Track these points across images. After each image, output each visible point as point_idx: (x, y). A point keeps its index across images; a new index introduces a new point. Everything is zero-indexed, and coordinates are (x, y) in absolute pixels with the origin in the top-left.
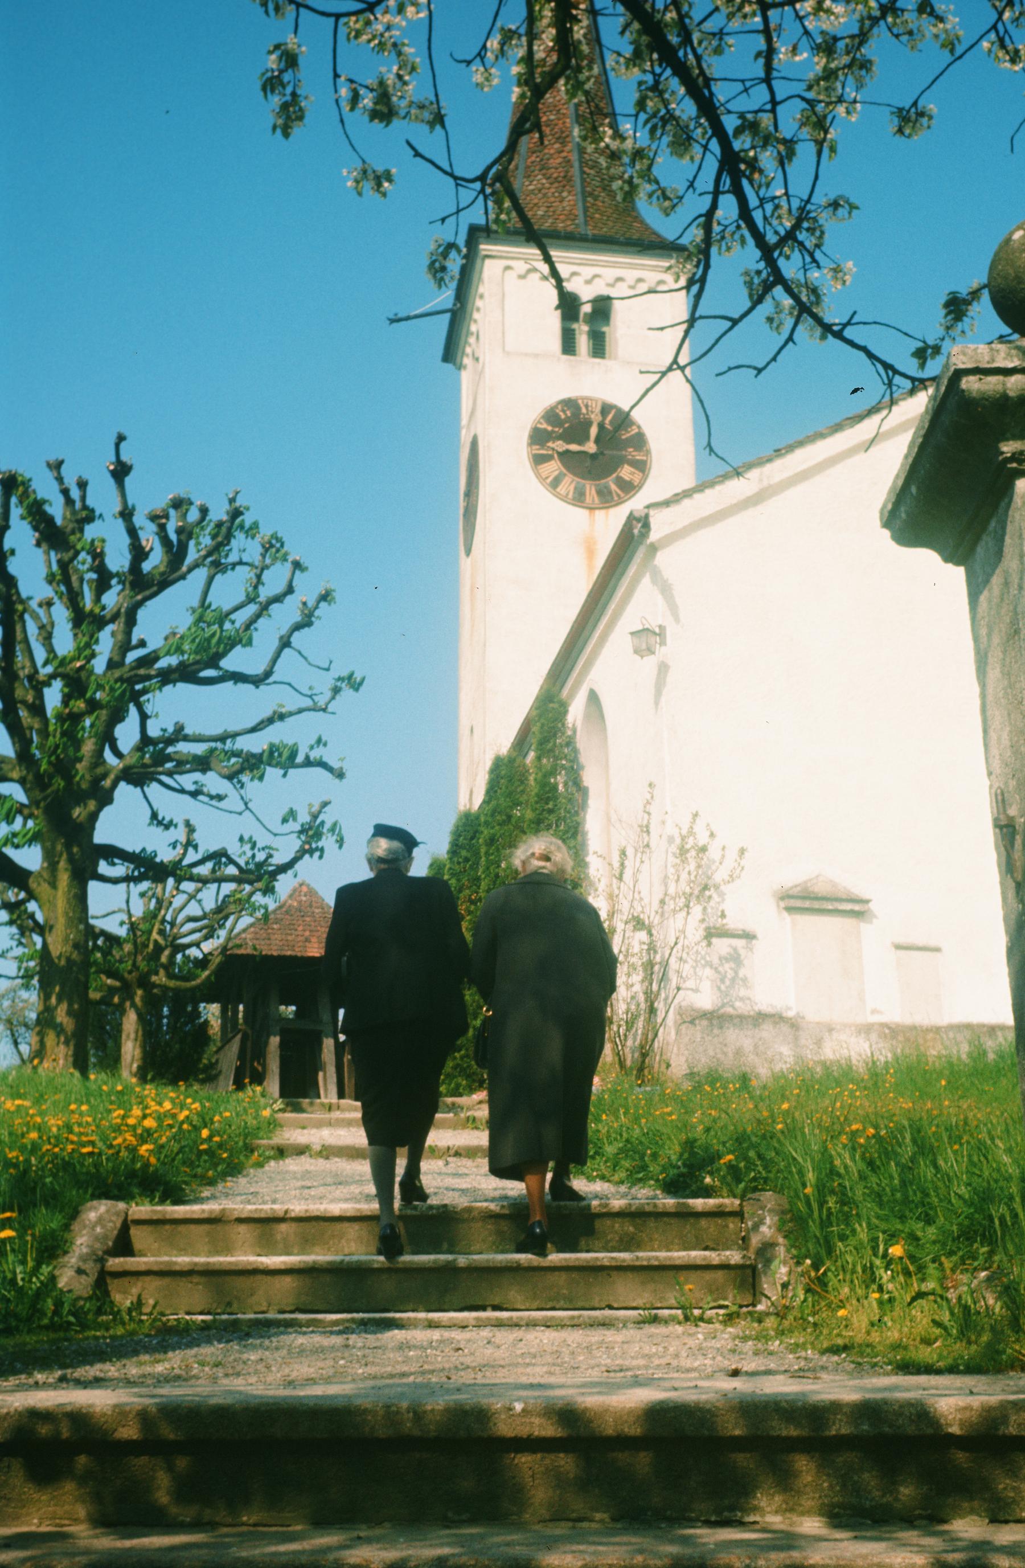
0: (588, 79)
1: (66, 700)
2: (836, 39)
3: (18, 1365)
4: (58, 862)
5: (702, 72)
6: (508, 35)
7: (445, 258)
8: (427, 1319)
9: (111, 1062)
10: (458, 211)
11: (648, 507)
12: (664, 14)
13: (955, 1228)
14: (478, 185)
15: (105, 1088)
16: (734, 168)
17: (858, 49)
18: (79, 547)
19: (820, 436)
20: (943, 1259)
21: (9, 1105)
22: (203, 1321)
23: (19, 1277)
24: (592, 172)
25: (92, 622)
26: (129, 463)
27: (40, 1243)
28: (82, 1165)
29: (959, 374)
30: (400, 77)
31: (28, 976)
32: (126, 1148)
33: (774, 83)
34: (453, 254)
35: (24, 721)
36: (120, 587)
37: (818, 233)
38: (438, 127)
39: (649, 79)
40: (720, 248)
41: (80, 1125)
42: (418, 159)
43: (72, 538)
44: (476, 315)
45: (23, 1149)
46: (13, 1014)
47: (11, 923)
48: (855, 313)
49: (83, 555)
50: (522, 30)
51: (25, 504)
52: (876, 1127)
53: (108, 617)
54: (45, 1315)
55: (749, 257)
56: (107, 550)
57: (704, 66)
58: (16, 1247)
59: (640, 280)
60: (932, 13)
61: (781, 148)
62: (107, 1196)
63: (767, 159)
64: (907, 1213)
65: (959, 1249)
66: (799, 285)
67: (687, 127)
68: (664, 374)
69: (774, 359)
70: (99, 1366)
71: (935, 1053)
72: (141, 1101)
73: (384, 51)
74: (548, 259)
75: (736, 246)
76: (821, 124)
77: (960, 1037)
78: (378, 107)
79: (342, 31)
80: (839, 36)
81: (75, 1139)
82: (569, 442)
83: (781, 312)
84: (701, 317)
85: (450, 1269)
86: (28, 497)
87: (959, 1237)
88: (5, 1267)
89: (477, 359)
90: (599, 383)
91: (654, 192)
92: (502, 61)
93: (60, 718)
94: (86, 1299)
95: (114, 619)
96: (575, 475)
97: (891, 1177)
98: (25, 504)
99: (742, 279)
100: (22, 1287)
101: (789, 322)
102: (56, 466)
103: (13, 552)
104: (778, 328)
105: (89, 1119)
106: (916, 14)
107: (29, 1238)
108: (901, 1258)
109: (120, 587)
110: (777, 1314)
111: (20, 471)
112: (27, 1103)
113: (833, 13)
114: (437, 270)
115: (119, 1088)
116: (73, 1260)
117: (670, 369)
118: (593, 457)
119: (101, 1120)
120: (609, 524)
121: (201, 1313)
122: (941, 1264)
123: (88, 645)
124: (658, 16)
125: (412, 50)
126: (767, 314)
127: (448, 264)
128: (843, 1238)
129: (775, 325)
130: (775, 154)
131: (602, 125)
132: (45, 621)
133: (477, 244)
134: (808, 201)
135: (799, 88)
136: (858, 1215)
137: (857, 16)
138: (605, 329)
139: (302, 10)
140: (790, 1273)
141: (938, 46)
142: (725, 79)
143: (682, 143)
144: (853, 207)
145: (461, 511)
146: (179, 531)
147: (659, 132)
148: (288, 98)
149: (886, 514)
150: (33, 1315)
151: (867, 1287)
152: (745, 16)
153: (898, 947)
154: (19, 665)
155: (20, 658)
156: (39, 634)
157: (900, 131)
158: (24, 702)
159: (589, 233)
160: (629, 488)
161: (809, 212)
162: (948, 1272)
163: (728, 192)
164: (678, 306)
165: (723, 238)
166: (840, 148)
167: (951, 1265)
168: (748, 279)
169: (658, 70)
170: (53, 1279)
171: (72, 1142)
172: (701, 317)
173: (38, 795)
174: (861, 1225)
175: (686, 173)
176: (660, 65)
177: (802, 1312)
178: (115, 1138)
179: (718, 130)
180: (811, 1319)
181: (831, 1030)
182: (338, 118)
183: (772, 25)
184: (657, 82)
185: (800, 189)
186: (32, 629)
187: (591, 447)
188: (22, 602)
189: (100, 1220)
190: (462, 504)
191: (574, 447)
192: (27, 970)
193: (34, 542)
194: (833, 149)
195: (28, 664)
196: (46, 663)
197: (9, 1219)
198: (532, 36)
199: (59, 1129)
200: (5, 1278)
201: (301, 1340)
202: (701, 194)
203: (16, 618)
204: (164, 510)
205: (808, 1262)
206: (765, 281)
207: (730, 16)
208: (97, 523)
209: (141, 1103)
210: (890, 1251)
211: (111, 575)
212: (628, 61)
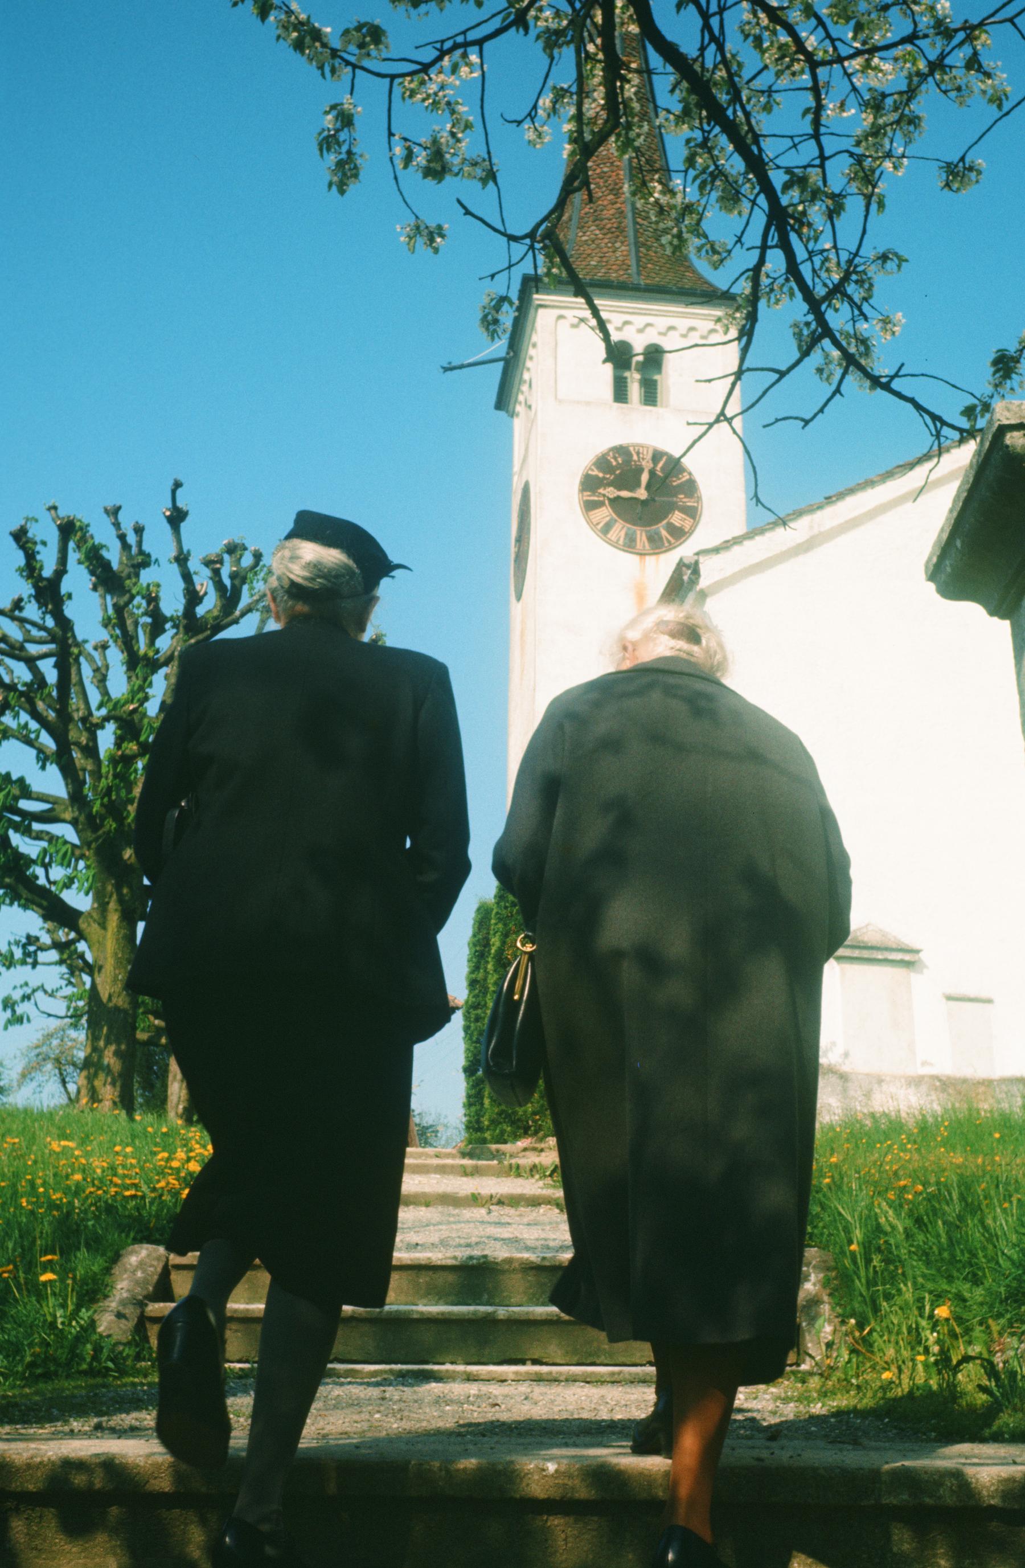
0: (639, 135)
1: (119, 742)
2: (884, 96)
3: (55, 1412)
4: (108, 903)
5: (751, 129)
6: (560, 94)
7: (497, 312)
8: (465, 1372)
9: (158, 1103)
10: (509, 267)
11: (697, 554)
12: (713, 73)
13: (1002, 1289)
14: (528, 241)
15: (150, 1129)
16: (781, 220)
17: (907, 104)
18: (134, 591)
19: (870, 483)
20: (990, 1321)
21: (55, 1146)
22: (241, 1369)
23: (60, 1320)
24: (645, 223)
25: (147, 665)
26: (185, 509)
27: (81, 1287)
28: (124, 1207)
29: (1003, 430)
30: (453, 135)
31: (76, 1016)
32: (169, 1191)
33: (823, 138)
34: (506, 307)
35: (77, 762)
36: (175, 631)
37: (866, 286)
38: (491, 184)
39: (698, 135)
40: (769, 301)
41: (124, 1166)
42: (468, 217)
43: (128, 582)
44: (529, 364)
45: (66, 1191)
46: (62, 1053)
47: (61, 962)
48: (903, 365)
49: (138, 600)
50: (574, 89)
51: (83, 550)
52: (925, 1184)
53: (162, 660)
54: (84, 1359)
55: (797, 309)
56: (162, 595)
57: (753, 122)
58: (57, 1291)
59: (692, 329)
60: (980, 69)
61: (830, 202)
62: (149, 1239)
63: (816, 213)
64: (955, 1274)
65: (1007, 1311)
66: (848, 336)
67: (736, 182)
68: (711, 425)
69: (821, 411)
70: (135, 1414)
71: (986, 1107)
72: (186, 1143)
73: (438, 109)
74: (595, 312)
75: (785, 298)
76: (867, 178)
77: (1014, 1089)
78: (432, 165)
79: (397, 91)
80: (887, 92)
81: (119, 1182)
82: (619, 490)
83: (831, 362)
84: (749, 370)
85: (490, 1322)
86: (86, 542)
87: (1007, 1299)
88: (45, 1309)
89: (530, 407)
90: (648, 431)
91: (703, 246)
92: (554, 119)
93: (113, 760)
94: (125, 1344)
95: (166, 663)
96: (626, 521)
97: (938, 1236)
98: (83, 550)
99: (791, 331)
100: (61, 1330)
101: (838, 372)
102: (114, 512)
103: (70, 596)
104: (828, 379)
105: (134, 1161)
106: (964, 70)
107: (70, 1282)
108: (947, 1320)
109: (175, 631)
110: (821, 1375)
111: (79, 517)
112: (70, 1144)
113: (881, 71)
114: (490, 323)
115: (164, 1130)
116: (114, 1305)
117: (717, 421)
118: (644, 503)
119: (145, 1162)
120: (661, 568)
121: (239, 1361)
122: (988, 1327)
123: (141, 688)
124: (708, 75)
125: (465, 109)
126: (816, 365)
127: (501, 317)
128: (888, 1297)
129: (825, 376)
130: (824, 208)
131: (652, 180)
132: (100, 664)
133: (531, 294)
134: (856, 254)
135: (848, 144)
136: (904, 1274)
137: (905, 73)
138: (656, 377)
139: (357, 71)
140: (835, 1332)
141: (986, 101)
142: (774, 135)
143: (731, 198)
144: (901, 260)
145: (513, 556)
146: (233, 576)
147: (708, 187)
148: (344, 156)
149: (931, 568)
150: (72, 1359)
151: (912, 1349)
152: (794, 74)
153: (950, 998)
154: (74, 707)
155: (75, 701)
156: (94, 677)
157: (948, 185)
158: (77, 744)
159: (642, 282)
160: (679, 534)
161: (856, 266)
162: (995, 1335)
163: (776, 246)
164: (729, 357)
165: (772, 290)
166: (887, 202)
167: (998, 1328)
168: (797, 330)
169: (706, 128)
170: (92, 1324)
171: (116, 1185)
172: (749, 370)
173: (89, 835)
174: (906, 1285)
175: (733, 229)
176: (709, 124)
177: (846, 1374)
178: (159, 1181)
179: (767, 187)
180: (854, 1381)
181: (880, 1081)
182: (393, 176)
183: (821, 84)
184: (706, 140)
185: (848, 241)
186: (87, 671)
187: (642, 494)
188: (77, 645)
189: (141, 1265)
190: (513, 550)
191: (625, 494)
192: (76, 1009)
193: (91, 586)
194: (881, 205)
195: (82, 706)
196: (100, 706)
197: (50, 1261)
198: (582, 93)
199: (103, 1171)
200: (45, 1321)
201: (337, 1391)
202: (748, 249)
203: (71, 660)
204: (218, 555)
205: (853, 1321)
206: (814, 332)
207: (778, 74)
208: (153, 568)
209: (185, 1146)
210: (936, 1312)
211: (165, 620)
212: (677, 117)
